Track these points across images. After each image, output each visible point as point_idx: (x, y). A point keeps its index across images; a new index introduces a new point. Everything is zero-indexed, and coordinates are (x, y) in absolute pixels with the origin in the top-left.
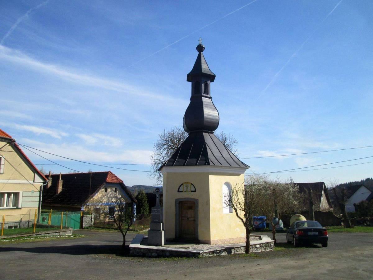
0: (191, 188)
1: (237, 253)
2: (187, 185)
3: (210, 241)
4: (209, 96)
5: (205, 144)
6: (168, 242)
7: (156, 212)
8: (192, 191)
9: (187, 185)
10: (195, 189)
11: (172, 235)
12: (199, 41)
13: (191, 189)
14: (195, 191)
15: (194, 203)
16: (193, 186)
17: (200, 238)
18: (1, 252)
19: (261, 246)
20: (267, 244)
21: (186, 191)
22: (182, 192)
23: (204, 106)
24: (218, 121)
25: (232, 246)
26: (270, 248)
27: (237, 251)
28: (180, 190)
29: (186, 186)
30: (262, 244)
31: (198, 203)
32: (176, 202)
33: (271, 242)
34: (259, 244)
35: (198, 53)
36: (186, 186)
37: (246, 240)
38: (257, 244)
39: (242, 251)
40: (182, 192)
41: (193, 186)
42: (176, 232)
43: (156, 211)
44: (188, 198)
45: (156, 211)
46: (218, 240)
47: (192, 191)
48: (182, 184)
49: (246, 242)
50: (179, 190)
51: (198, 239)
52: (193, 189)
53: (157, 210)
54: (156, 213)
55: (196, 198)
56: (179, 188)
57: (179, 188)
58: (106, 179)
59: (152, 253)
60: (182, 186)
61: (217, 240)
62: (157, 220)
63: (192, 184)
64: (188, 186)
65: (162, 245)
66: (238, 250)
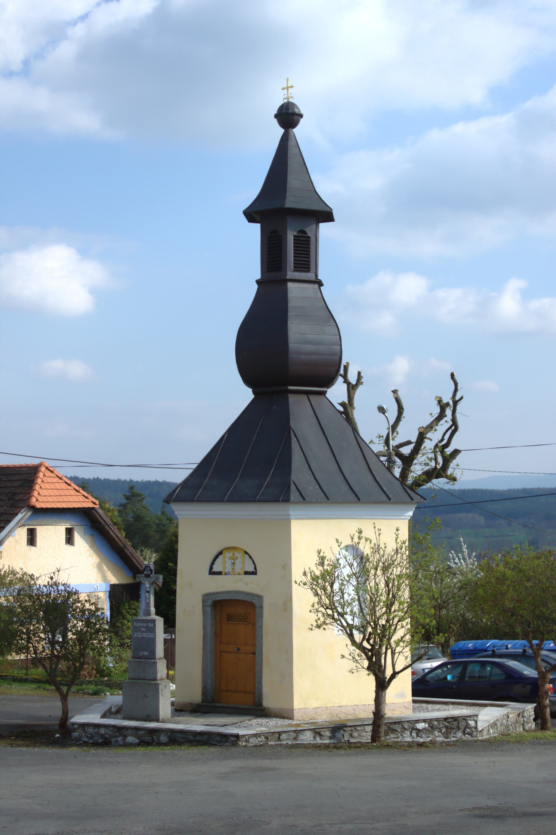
0: (243, 563)
1: (352, 740)
2: (234, 554)
3: (293, 710)
4: (310, 276)
5: (289, 432)
6: (179, 709)
7: (143, 632)
8: (246, 573)
9: (234, 554)
10: (255, 568)
11: (195, 695)
12: (283, 89)
13: (244, 567)
14: (254, 573)
15: (251, 605)
16: (250, 557)
17: (268, 702)
18: (555, 489)
19: (432, 727)
20: (455, 723)
21: (230, 571)
22: (220, 573)
23: (291, 313)
24: (339, 358)
25: (345, 723)
26: (464, 734)
27: (351, 735)
28: (216, 569)
29: (230, 558)
30: (437, 720)
31: (262, 608)
32: (204, 601)
33: (470, 716)
34: (424, 721)
35: (282, 131)
36: (230, 558)
37: (373, 708)
38: (418, 721)
39: (366, 736)
40: (220, 573)
41: (250, 557)
42: (204, 688)
43: (144, 629)
44: (236, 592)
45: (144, 629)
46: (318, 708)
47: (246, 573)
48: (221, 553)
49: (374, 713)
50: (211, 568)
51: (260, 704)
52: (251, 569)
53: (145, 625)
54: (144, 635)
55: (257, 591)
56: (213, 563)
57: (213, 563)
58: (29, 498)
59: (125, 736)
60: (221, 557)
61: (315, 708)
62: (146, 653)
63: (246, 553)
64: (237, 558)
65: (159, 720)
66: (356, 734)
